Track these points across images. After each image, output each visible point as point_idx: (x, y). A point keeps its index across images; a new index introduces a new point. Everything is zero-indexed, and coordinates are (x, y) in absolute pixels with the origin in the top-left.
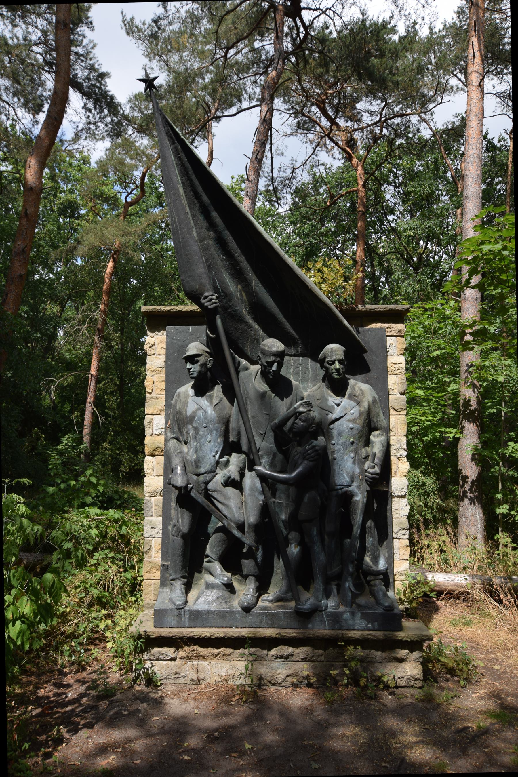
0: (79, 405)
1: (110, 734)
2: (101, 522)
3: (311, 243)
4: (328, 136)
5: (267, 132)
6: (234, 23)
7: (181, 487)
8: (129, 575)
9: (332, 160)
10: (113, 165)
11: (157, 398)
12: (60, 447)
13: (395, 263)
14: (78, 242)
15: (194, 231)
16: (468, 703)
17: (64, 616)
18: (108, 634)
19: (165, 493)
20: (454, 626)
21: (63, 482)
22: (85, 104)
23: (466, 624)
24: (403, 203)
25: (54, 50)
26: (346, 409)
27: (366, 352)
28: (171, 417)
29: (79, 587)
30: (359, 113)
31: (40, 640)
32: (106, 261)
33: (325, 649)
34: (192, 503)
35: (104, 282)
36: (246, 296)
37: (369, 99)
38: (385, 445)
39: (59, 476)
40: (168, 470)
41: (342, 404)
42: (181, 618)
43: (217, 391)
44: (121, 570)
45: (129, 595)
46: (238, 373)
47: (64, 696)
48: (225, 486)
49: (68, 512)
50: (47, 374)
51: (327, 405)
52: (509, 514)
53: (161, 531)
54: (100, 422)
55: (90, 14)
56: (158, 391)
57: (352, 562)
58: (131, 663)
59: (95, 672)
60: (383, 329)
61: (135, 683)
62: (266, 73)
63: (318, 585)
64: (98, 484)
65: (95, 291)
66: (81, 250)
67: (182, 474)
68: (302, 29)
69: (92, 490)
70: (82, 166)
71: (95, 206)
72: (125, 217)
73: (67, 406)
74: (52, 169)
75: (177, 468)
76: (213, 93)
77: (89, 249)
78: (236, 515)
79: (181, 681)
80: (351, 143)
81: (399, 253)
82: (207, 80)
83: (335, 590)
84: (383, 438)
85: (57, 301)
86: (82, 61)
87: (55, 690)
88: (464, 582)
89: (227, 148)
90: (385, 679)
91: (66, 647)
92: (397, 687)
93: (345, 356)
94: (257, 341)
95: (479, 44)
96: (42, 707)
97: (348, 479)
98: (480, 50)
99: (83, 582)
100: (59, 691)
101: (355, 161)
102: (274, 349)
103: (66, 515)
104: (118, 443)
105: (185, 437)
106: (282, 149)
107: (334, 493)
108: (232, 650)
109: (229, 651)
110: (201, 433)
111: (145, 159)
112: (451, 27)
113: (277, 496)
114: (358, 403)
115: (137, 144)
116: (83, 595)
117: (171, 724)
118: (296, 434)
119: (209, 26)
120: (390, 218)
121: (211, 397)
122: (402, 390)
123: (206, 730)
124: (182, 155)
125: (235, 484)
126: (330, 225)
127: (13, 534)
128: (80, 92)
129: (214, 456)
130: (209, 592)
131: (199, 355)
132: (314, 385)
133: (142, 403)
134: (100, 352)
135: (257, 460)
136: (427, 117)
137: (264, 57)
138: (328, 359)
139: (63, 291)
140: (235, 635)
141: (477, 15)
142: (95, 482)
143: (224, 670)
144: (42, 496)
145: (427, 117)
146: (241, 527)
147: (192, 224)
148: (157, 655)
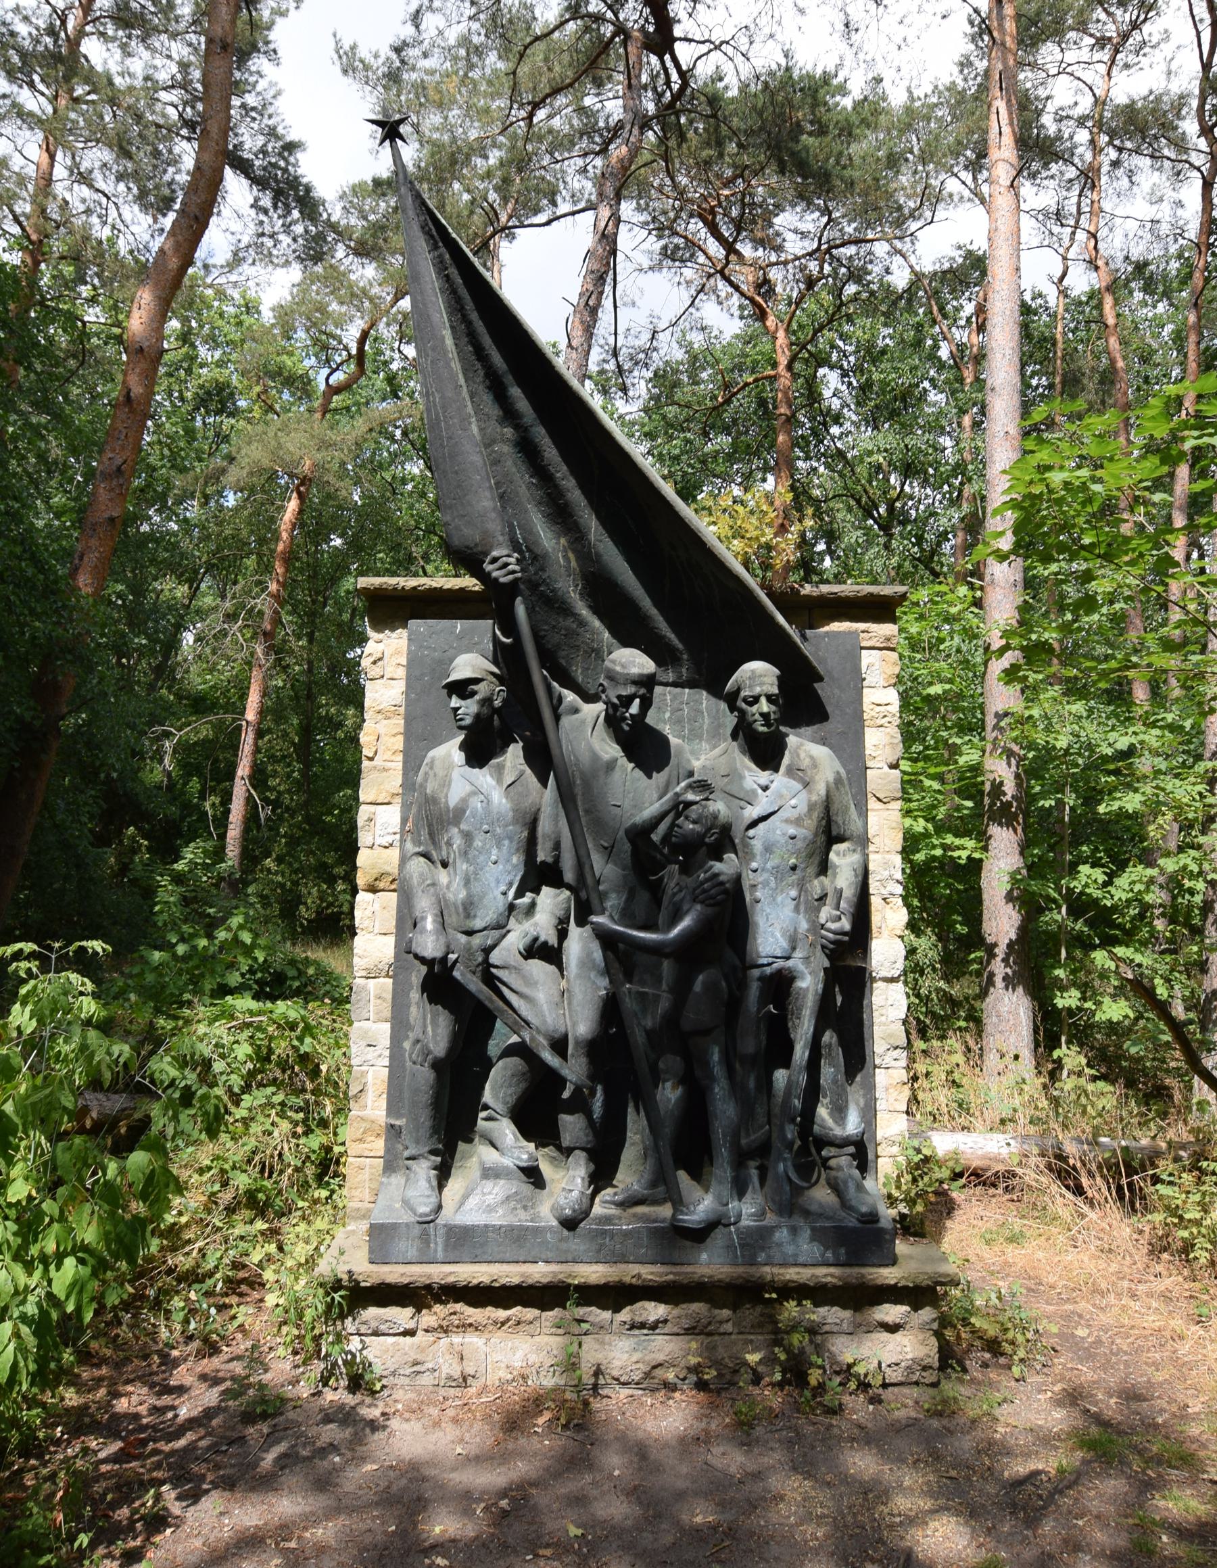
0: (219, 783)
1: (271, 1505)
2: (259, 1028)
3: (685, 474)
4: (722, 272)
5: (608, 258)
6: (546, 59)
7: (434, 960)
8: (315, 1141)
9: (724, 321)
10: (303, 312)
11: (385, 770)
12: (180, 866)
13: (843, 516)
14: (231, 459)
15: (474, 430)
16: (1032, 1416)
17: (174, 1232)
18: (268, 1275)
19: (397, 970)
20: (988, 1243)
21: (182, 940)
22: (257, 200)
23: (1011, 1240)
24: (858, 404)
25: (200, 99)
26: (781, 796)
27: (821, 679)
28: (414, 809)
29: (210, 1168)
30: (778, 234)
31: (122, 1285)
32: (285, 498)
33: (735, 1308)
34: (459, 995)
35: (277, 538)
36: (578, 559)
37: (798, 209)
38: (860, 871)
39: (175, 926)
40: (407, 921)
41: (773, 786)
42: (428, 1243)
43: (514, 756)
44: (299, 1130)
45: (314, 1185)
46: (557, 718)
47: (170, 1415)
48: (526, 958)
49: (190, 1004)
50: (155, 720)
51: (742, 788)
52: (1079, 1009)
53: (387, 1053)
54: (262, 816)
55: (272, 36)
56: (388, 756)
57: (793, 1120)
58: (317, 1339)
59: (238, 1358)
60: (855, 634)
61: (326, 1384)
62: (604, 151)
63: (722, 1170)
64: (254, 945)
65: (260, 556)
66: (235, 474)
67: (436, 932)
68: (675, 76)
69: (241, 959)
70: (244, 317)
71: (265, 391)
72: (324, 415)
73: (195, 784)
74: (185, 321)
75: (424, 918)
76: (504, 188)
77: (251, 474)
78: (549, 1020)
79: (426, 1380)
80: (765, 286)
81: (852, 496)
82: (492, 161)
83: (756, 1180)
84: (856, 858)
85: (182, 574)
86: (254, 119)
87: (152, 1400)
88: (1005, 1151)
89: (538, 275)
90: (860, 1369)
91: (177, 1302)
92: (885, 1385)
93: (780, 687)
94: (597, 654)
95: (1010, 113)
96: (122, 1439)
97: (784, 944)
98: (1011, 124)
99: (216, 1158)
100: (159, 1403)
101: (771, 322)
102: (635, 671)
103: (187, 1012)
104: (298, 859)
105: (444, 853)
106: (633, 294)
107: (756, 973)
108: (537, 1312)
109: (530, 1313)
110: (478, 843)
111: (367, 304)
112: (948, 89)
113: (636, 978)
114: (806, 785)
115: (353, 277)
116: (217, 1187)
117: (404, 1481)
118: (677, 849)
119: (501, 65)
120: (835, 430)
121: (500, 769)
122: (892, 759)
123: (483, 1493)
124: (453, 272)
125: (546, 952)
126: (722, 441)
127: (66, 1060)
128: (247, 176)
129: (505, 894)
130: (488, 1185)
131: (477, 681)
132: (715, 747)
133: (352, 779)
134: (267, 677)
135: (595, 901)
136: (905, 246)
137: (601, 124)
138: (745, 693)
139: (201, 555)
140: (545, 1280)
141: (1005, 61)
142: (248, 941)
143: (520, 1354)
144: (136, 970)
145: (905, 246)
146: (559, 1045)
147: (470, 409)
148: (374, 1324)
